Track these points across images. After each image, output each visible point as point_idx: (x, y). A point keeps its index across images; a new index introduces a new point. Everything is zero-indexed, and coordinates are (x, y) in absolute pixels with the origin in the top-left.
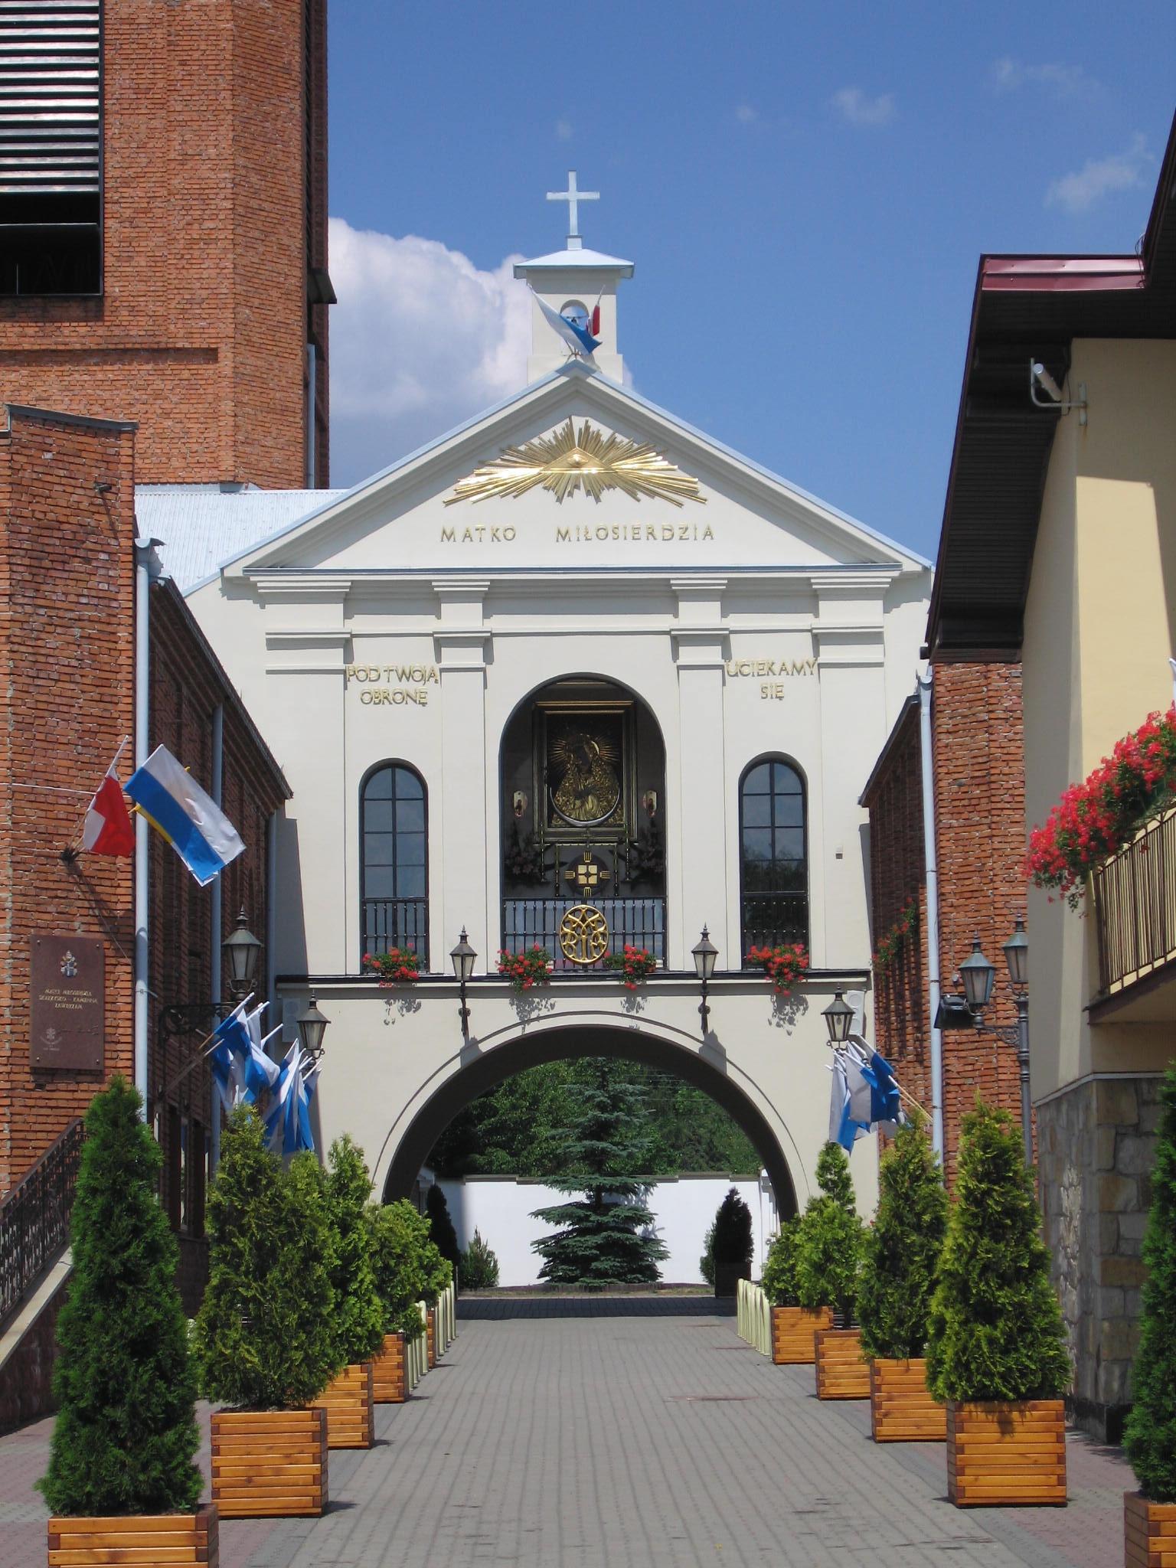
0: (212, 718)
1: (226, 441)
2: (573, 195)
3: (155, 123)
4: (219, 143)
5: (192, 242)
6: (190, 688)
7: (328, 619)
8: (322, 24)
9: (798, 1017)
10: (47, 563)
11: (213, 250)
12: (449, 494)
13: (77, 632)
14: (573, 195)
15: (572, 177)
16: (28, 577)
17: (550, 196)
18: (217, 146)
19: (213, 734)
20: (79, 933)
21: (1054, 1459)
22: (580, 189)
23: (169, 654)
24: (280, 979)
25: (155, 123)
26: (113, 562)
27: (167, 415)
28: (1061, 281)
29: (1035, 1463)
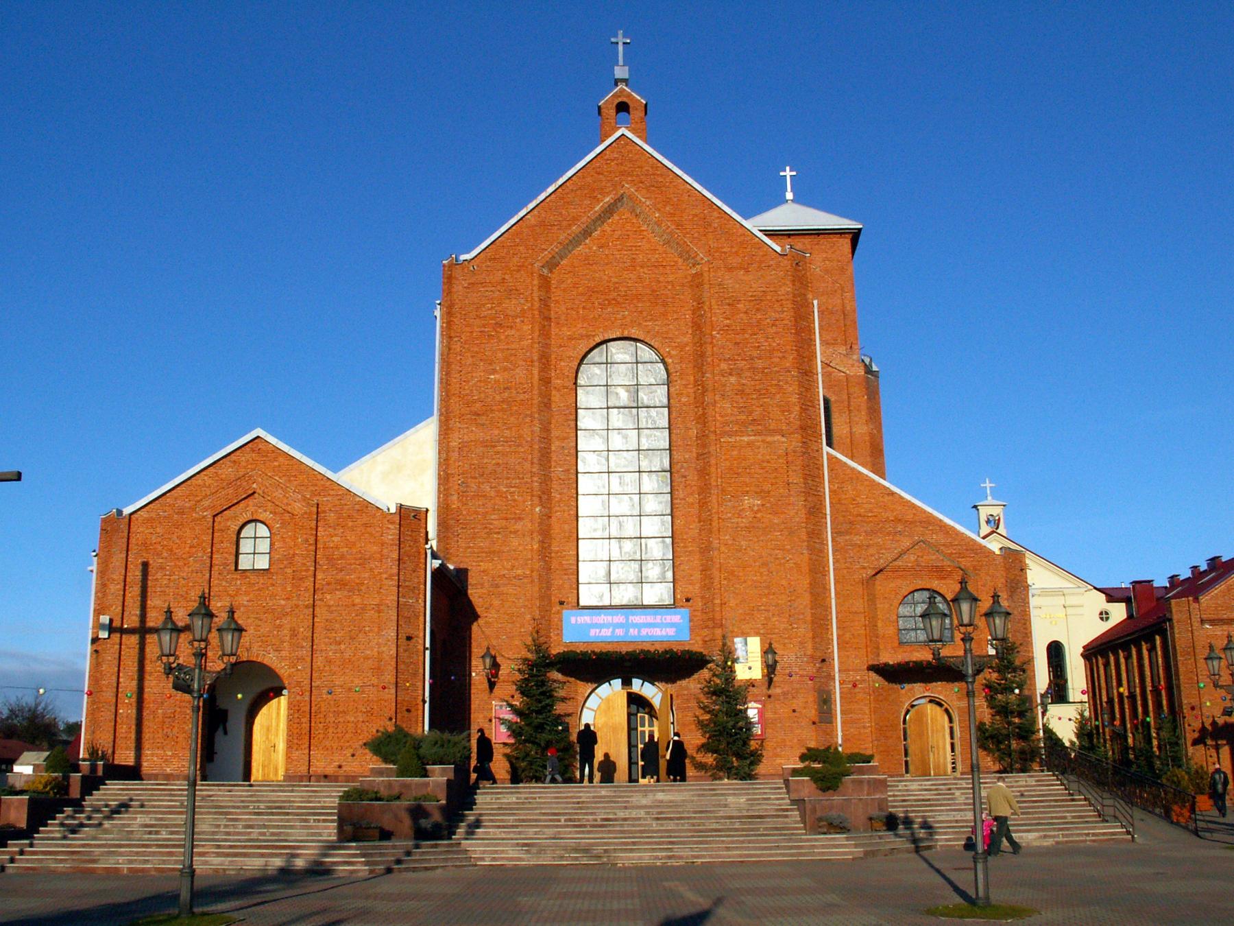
14: (988, 485)
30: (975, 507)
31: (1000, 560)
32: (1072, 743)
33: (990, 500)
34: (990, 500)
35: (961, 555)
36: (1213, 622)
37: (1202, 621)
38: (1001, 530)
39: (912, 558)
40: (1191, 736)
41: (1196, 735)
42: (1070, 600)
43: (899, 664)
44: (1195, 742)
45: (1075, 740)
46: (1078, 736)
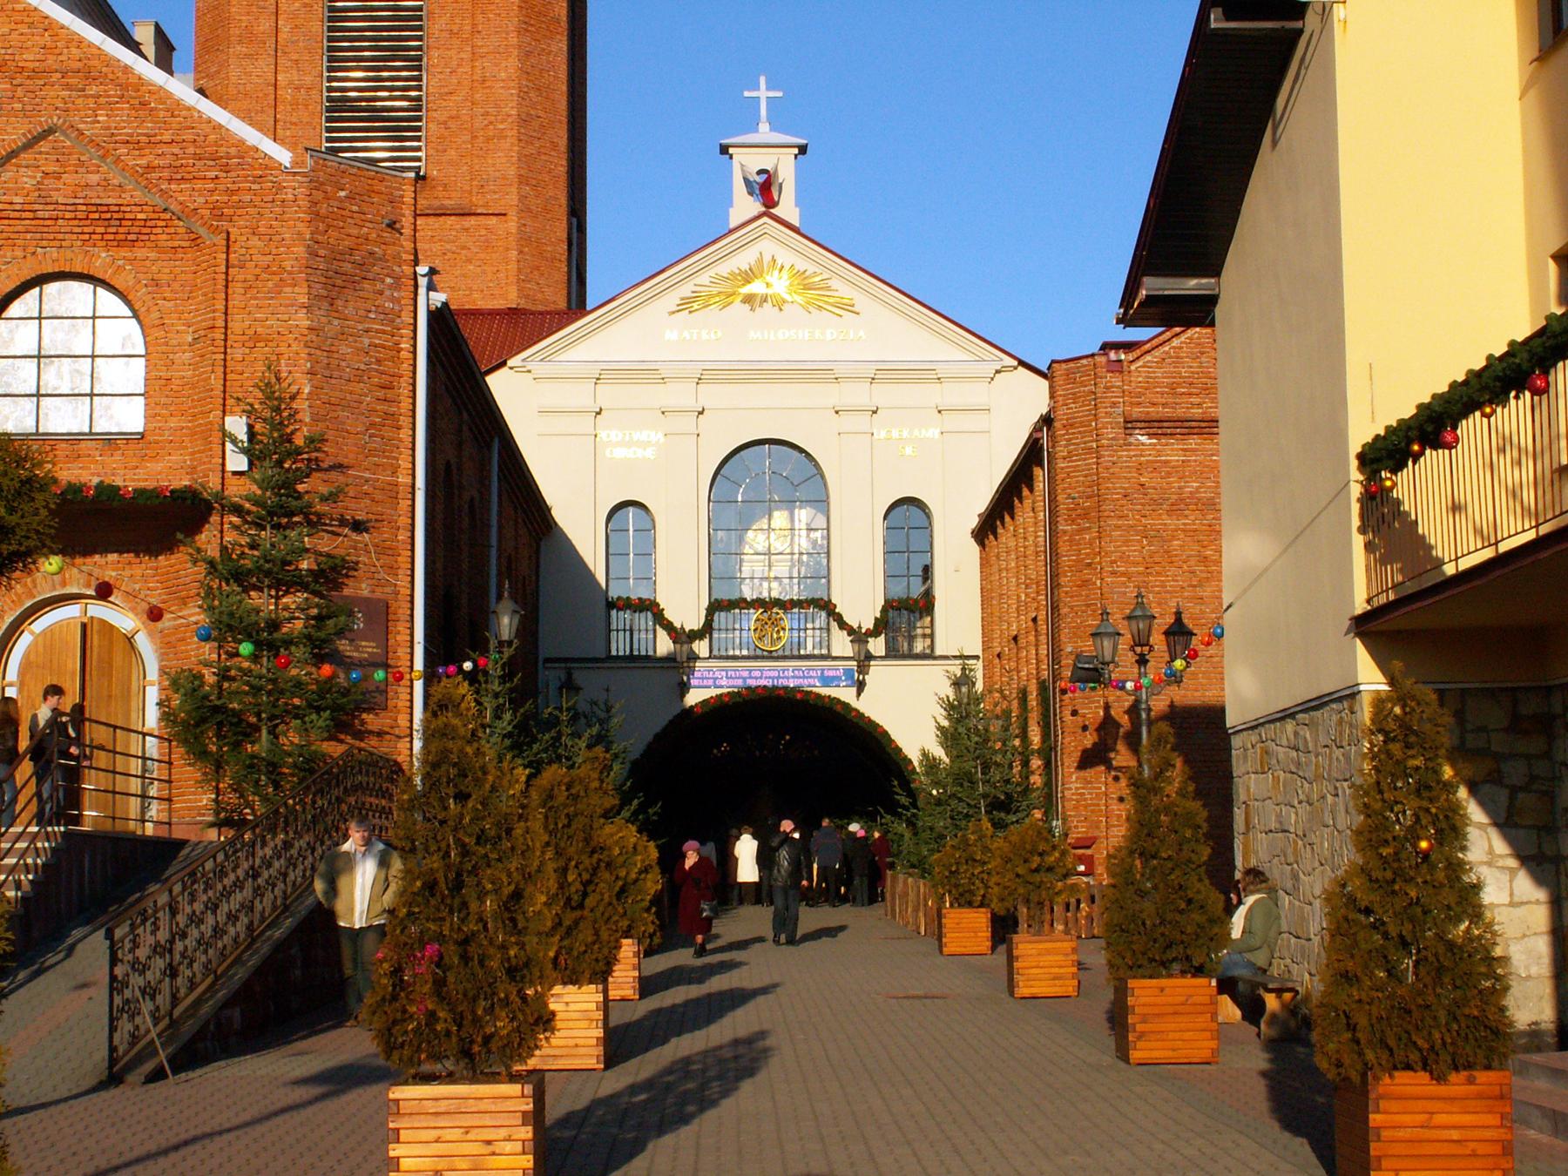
0: (489, 447)
1: (513, 279)
2: (763, 93)
3: (463, 55)
4: (509, 67)
5: (488, 140)
6: (470, 415)
7: (581, 395)
8: (583, 58)
9: (950, 692)
10: (339, 282)
11: (506, 144)
12: (672, 299)
13: (366, 341)
14: (763, 93)
15: (762, 80)
16: (324, 293)
17: (746, 94)
18: (506, 70)
19: (490, 459)
20: (366, 593)
21: (1497, 1149)
22: (768, 89)
23: (449, 378)
24: (547, 660)
25: (463, 55)
26: (397, 285)
27: (469, 261)
28: (504, 1165)
29: (1474, 1155)
30: (724, 150)
31: (296, 189)
32: (930, 763)
33: (764, 133)
34: (764, 133)
35: (178, 173)
36: (1156, 426)
37: (1130, 424)
38: (787, 208)
39: (28, 180)
40: (1073, 743)
41: (1089, 740)
42: (951, 394)
43: (140, 492)
44: (1089, 759)
45: (939, 752)
46: (948, 737)
